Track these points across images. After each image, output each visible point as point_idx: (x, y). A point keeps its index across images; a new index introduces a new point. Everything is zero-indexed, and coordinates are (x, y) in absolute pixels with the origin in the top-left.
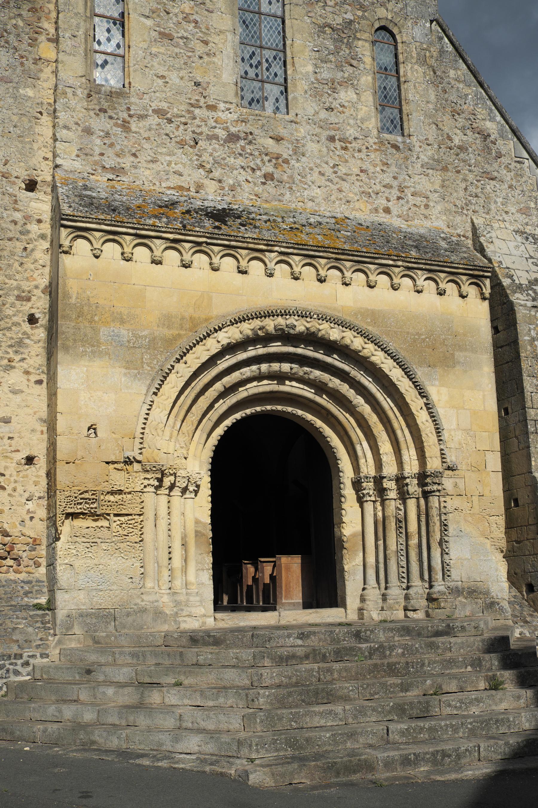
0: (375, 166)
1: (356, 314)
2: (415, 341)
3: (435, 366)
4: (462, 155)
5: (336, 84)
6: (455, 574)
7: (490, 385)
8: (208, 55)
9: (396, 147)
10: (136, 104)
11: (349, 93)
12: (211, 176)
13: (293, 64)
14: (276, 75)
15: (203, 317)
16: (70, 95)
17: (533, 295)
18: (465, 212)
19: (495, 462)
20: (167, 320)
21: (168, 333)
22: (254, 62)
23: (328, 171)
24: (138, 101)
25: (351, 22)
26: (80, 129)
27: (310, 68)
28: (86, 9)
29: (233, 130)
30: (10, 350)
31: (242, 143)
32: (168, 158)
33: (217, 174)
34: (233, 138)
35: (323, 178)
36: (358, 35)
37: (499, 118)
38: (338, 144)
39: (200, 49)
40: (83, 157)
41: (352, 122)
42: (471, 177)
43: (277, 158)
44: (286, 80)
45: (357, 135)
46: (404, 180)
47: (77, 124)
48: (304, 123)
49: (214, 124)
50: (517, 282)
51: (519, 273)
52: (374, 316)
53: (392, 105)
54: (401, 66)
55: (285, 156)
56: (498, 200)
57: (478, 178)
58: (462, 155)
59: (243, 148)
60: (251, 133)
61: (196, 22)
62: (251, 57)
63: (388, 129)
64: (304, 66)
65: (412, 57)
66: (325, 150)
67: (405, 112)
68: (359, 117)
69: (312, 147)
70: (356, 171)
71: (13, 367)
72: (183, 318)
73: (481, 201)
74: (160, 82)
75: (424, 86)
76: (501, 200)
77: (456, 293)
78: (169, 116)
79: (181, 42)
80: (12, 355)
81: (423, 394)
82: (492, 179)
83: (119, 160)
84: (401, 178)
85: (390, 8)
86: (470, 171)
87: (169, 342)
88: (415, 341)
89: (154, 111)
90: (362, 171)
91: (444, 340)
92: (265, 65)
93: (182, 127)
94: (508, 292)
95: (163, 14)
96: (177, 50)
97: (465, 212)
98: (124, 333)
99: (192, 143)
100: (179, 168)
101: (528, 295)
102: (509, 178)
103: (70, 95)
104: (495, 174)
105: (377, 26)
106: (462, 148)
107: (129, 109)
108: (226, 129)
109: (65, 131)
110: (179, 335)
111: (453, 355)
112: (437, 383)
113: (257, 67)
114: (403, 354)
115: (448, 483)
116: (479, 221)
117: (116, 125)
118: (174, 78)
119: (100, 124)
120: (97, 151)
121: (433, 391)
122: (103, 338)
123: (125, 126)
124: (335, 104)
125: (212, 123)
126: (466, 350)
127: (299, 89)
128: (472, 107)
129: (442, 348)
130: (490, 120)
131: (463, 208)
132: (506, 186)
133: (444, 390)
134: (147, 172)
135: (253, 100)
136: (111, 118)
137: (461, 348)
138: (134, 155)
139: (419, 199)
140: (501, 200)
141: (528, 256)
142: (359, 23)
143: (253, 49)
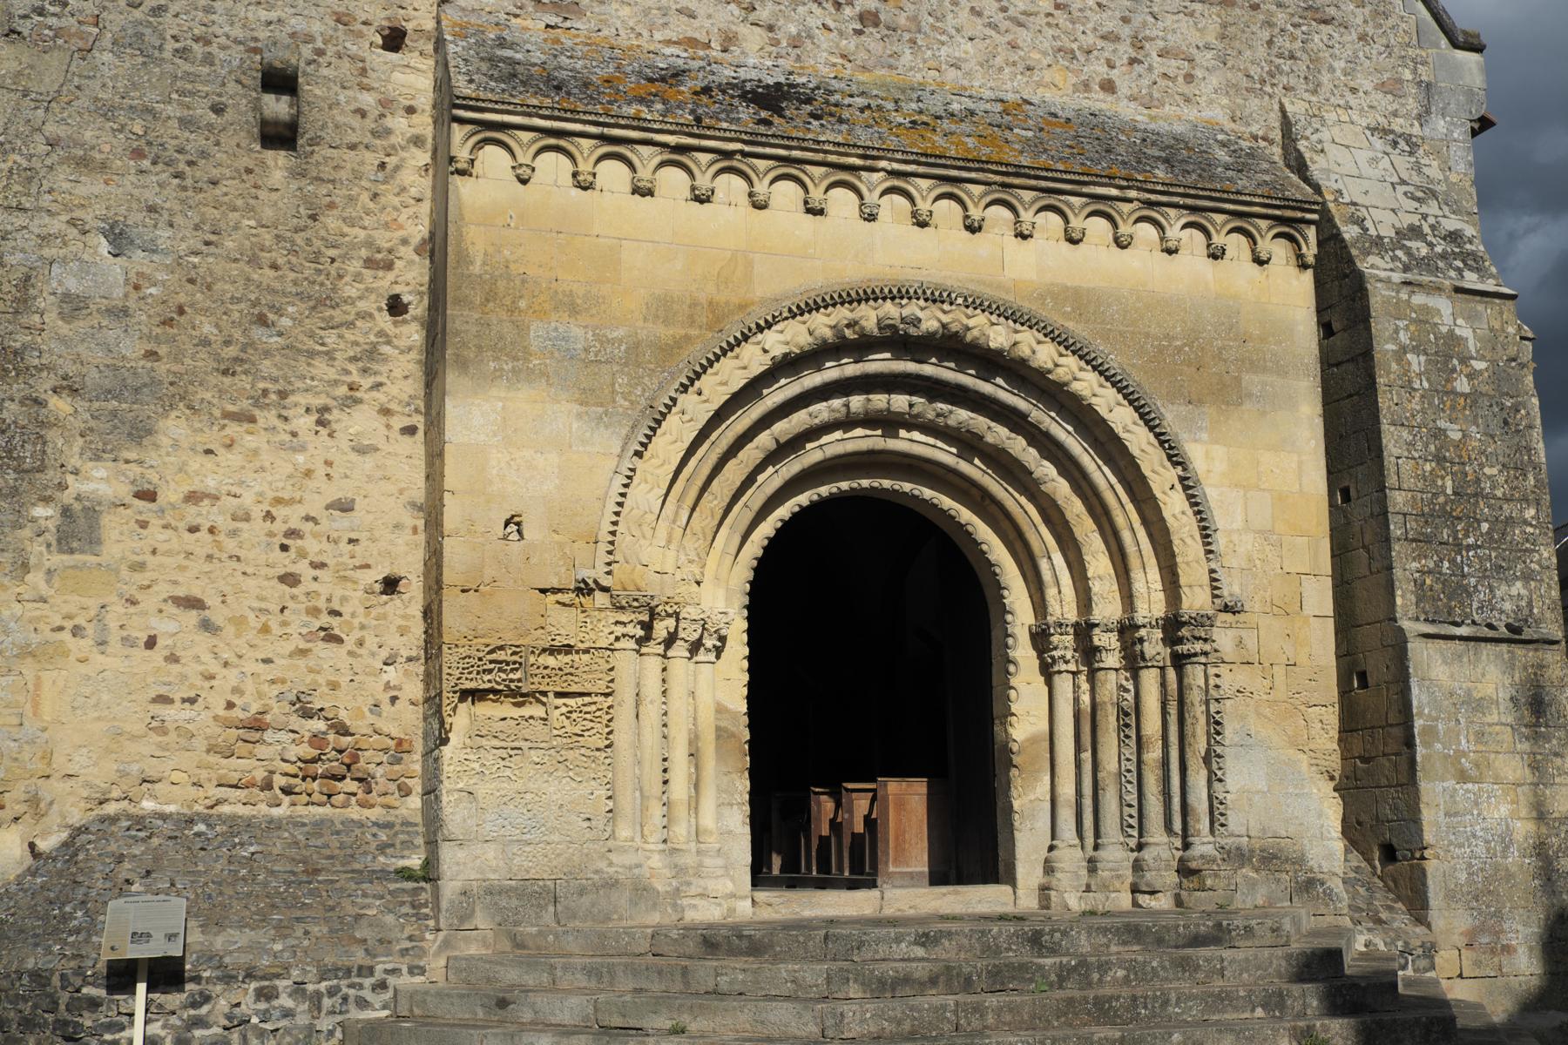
1: (1042, 297)
3: (1201, 402)
6: (1235, 822)
12: (752, 17)
15: (735, 300)
17: (1404, 258)
18: (1268, 89)
19: (1320, 597)
20: (663, 308)
21: (665, 333)
30: (352, 367)
35: (979, 21)
46: (1145, 24)
50: (1372, 232)
52: (1078, 299)
56: (1336, 64)
57: (1296, 20)
72: (694, 304)
73: (1302, 67)
76: (1343, 64)
77: (1247, 254)
80: (355, 377)
81: (1175, 458)
82: (1325, 22)
84: (1137, 20)
87: (667, 351)
94: (1354, 252)
97: (1268, 89)
98: (578, 333)
102: (1359, 20)
104: (1332, 11)
111: (1238, 380)
112: (1205, 436)
114: (1137, 378)
115: (1224, 638)
116: (1295, 108)
126: (1265, 370)
129: (1215, 367)
137: (1255, 366)
139: (1174, 63)
141: (1395, 179)
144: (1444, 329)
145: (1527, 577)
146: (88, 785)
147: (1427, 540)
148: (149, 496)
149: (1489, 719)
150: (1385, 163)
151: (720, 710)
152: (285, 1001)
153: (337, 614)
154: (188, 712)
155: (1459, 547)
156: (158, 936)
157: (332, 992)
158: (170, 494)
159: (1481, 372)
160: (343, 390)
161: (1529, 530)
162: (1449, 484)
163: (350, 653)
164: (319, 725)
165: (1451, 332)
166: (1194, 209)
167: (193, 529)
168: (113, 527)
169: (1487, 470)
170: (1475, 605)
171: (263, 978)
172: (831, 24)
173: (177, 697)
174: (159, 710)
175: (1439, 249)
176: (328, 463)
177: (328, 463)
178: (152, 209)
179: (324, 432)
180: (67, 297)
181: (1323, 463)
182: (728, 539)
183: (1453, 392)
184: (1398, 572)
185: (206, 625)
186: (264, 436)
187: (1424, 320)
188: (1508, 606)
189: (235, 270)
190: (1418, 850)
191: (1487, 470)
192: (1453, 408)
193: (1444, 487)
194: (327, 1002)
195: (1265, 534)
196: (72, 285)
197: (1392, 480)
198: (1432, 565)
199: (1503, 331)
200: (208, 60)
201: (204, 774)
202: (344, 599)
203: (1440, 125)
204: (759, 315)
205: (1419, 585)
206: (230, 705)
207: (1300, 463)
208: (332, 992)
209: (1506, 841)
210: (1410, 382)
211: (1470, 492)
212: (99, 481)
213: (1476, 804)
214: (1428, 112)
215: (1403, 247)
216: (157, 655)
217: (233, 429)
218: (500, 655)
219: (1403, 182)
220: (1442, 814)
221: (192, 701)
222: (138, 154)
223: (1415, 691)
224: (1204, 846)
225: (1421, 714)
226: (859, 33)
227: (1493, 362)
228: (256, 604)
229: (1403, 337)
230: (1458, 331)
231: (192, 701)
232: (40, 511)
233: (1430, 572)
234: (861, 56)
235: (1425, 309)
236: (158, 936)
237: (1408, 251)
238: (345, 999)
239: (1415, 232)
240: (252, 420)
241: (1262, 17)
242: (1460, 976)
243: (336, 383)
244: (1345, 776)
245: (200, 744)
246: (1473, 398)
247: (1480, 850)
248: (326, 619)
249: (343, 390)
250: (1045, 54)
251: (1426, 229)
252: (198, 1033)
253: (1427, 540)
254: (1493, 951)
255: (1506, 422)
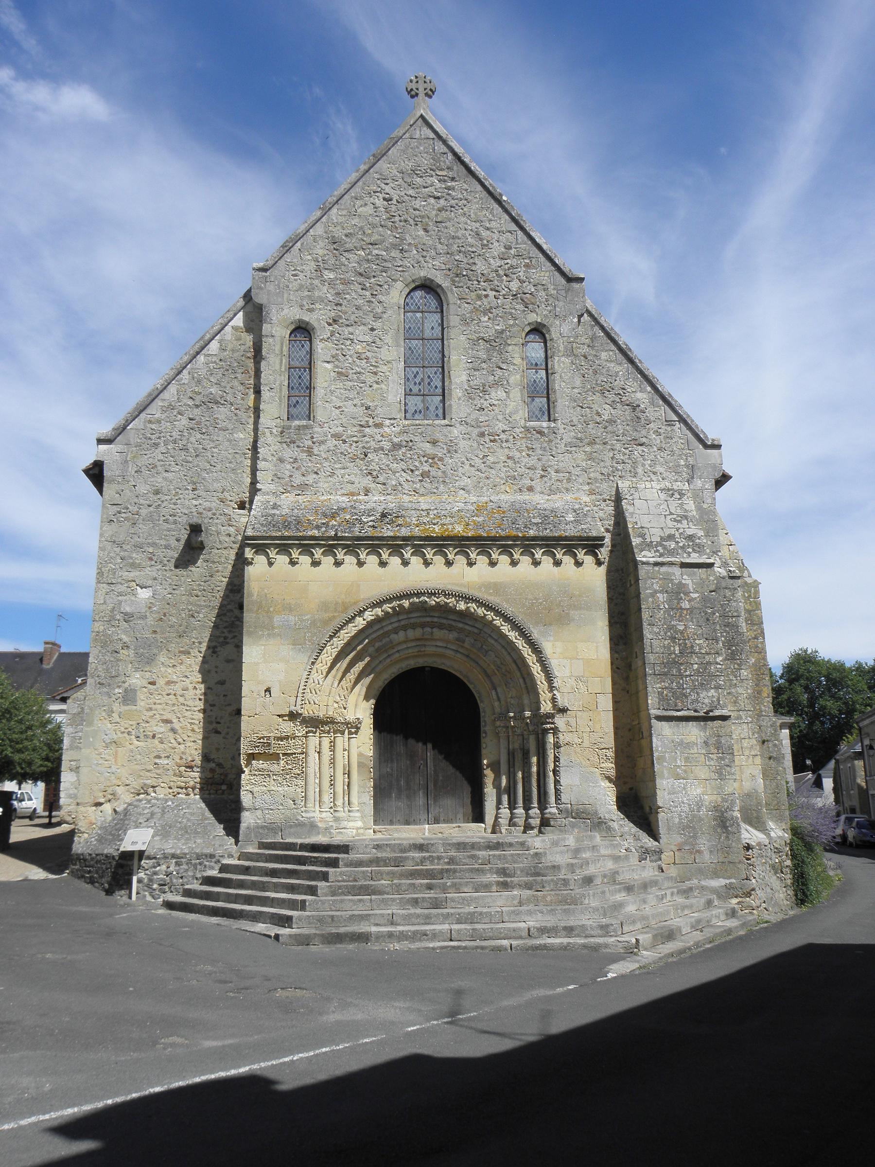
0: (521, 452)
1: (480, 588)
2: (532, 604)
3: (550, 624)
4: (610, 428)
5: (487, 387)
6: (564, 798)
7: (603, 638)
8: (377, 383)
9: (540, 433)
10: (318, 433)
11: (499, 393)
12: (377, 480)
13: (450, 378)
14: (436, 387)
15: (353, 601)
16: (268, 434)
17: (662, 551)
18: (611, 478)
19: (606, 703)
20: (324, 606)
21: (326, 616)
22: (418, 380)
23: (478, 462)
24: (320, 430)
25: (502, 332)
26: (275, 459)
27: (464, 378)
28: (281, 366)
29: (396, 440)
30: (225, 630)
31: (404, 450)
32: (342, 471)
33: (381, 479)
34: (396, 447)
35: (473, 469)
36: (509, 342)
37: (649, 389)
38: (487, 439)
39: (370, 379)
40: (277, 480)
41: (500, 417)
42: (618, 446)
43: (433, 458)
44: (444, 390)
45: (506, 428)
46: (549, 460)
47: (273, 455)
48: (458, 425)
49: (380, 438)
50: (648, 540)
51: (653, 531)
52: (497, 588)
53: (543, 396)
54: (549, 360)
55: (440, 455)
56: (646, 462)
57: (626, 446)
58: (610, 428)
59: (404, 454)
60: (411, 441)
61: (367, 358)
62: (415, 376)
63: (537, 416)
64: (459, 377)
65: (559, 351)
66: (475, 445)
67: (552, 400)
68: (507, 412)
69: (463, 444)
70: (504, 458)
71: (227, 643)
72: (337, 603)
73: (628, 467)
74: (337, 412)
75: (569, 375)
76: (649, 462)
77: (573, 561)
78: (344, 437)
79: (355, 376)
80: (226, 634)
81: (536, 650)
82: (641, 445)
83: (304, 478)
84: (545, 458)
85: (539, 313)
86: (618, 440)
87: (326, 622)
88: (532, 604)
89: (332, 436)
90: (508, 458)
91: (560, 602)
92: (427, 381)
93: (354, 444)
94: (636, 551)
95: (341, 357)
96: (351, 384)
97: (611, 478)
98: (292, 619)
99: (362, 456)
100: (352, 478)
101: (658, 551)
102: (658, 441)
103: (268, 434)
104: (644, 440)
105: (528, 329)
106: (612, 422)
107: (312, 438)
108: (391, 441)
109: (263, 463)
110: (334, 617)
111: (568, 614)
112: (552, 638)
113: (420, 384)
114: (520, 618)
115: (560, 721)
116: (624, 485)
117: (303, 451)
118: (349, 408)
119: (288, 453)
120: (288, 473)
121: (548, 647)
122: (276, 624)
123: (310, 452)
124: (486, 404)
125: (379, 437)
126: (581, 608)
127: (457, 393)
128: (622, 383)
129: (560, 611)
130: (641, 392)
131: (609, 475)
132: (655, 449)
133: (559, 644)
134: (326, 485)
135: (416, 411)
136: (298, 447)
137: (576, 608)
138: (316, 473)
139: (562, 474)
140: (649, 462)
141: (668, 513)
142: (509, 331)
143: (417, 369)
144: (676, 581)
145: (717, 687)
146: (134, 788)
147: (665, 674)
148: (153, 683)
149: (692, 751)
150: (664, 506)
151: (360, 755)
152: (185, 867)
153: (218, 723)
154: (166, 762)
155: (681, 676)
156: (140, 843)
157: (200, 864)
158: (161, 682)
159: (695, 598)
160: (222, 639)
161: (719, 666)
162: (677, 648)
163: (224, 738)
164: (213, 765)
165: (680, 582)
166: (547, 546)
167: (168, 695)
168: (141, 695)
169: (697, 642)
170: (689, 701)
171: (178, 858)
172: (409, 479)
173: (163, 756)
174: (157, 761)
175: (681, 544)
176: (216, 667)
177: (216, 667)
178: (155, 579)
179: (215, 655)
180: (126, 614)
181: (608, 645)
182: (361, 689)
183: (681, 608)
184: (650, 689)
185: (173, 730)
186: (193, 659)
187: (667, 578)
188: (706, 701)
189: (184, 598)
190: (655, 810)
191: (697, 642)
192: (681, 616)
193: (674, 650)
194: (199, 867)
195: (578, 679)
196: (128, 609)
197: (647, 649)
198: (667, 685)
199: (708, 579)
200: (175, 522)
201: (172, 784)
202: (221, 718)
203: (698, 483)
204: (361, 605)
205: (660, 694)
206: (181, 758)
207: (597, 647)
208: (200, 864)
209: (699, 805)
210: (659, 606)
211: (687, 651)
212: (136, 680)
213: (684, 788)
214: (693, 478)
215: (662, 545)
216: (156, 741)
217: (183, 657)
218: (262, 741)
219: (671, 514)
220: (666, 793)
221: (168, 757)
222: (151, 559)
223: (654, 740)
224: (552, 810)
225: (657, 750)
226: (421, 481)
227: (702, 593)
228: (190, 721)
229: (656, 587)
230: (684, 582)
231: (168, 757)
232: (117, 690)
233: (666, 688)
234: (422, 491)
235: (668, 574)
236: (140, 843)
237: (665, 548)
238: (205, 866)
239: (671, 537)
240: (189, 653)
241: (609, 447)
242: (674, 863)
243: (219, 637)
244: (618, 777)
245: (171, 773)
246: (691, 610)
247: (686, 809)
248: (214, 725)
249: (222, 639)
250: (502, 479)
251: (677, 535)
252: (155, 877)
253: (665, 674)
254: (691, 853)
255: (708, 620)
